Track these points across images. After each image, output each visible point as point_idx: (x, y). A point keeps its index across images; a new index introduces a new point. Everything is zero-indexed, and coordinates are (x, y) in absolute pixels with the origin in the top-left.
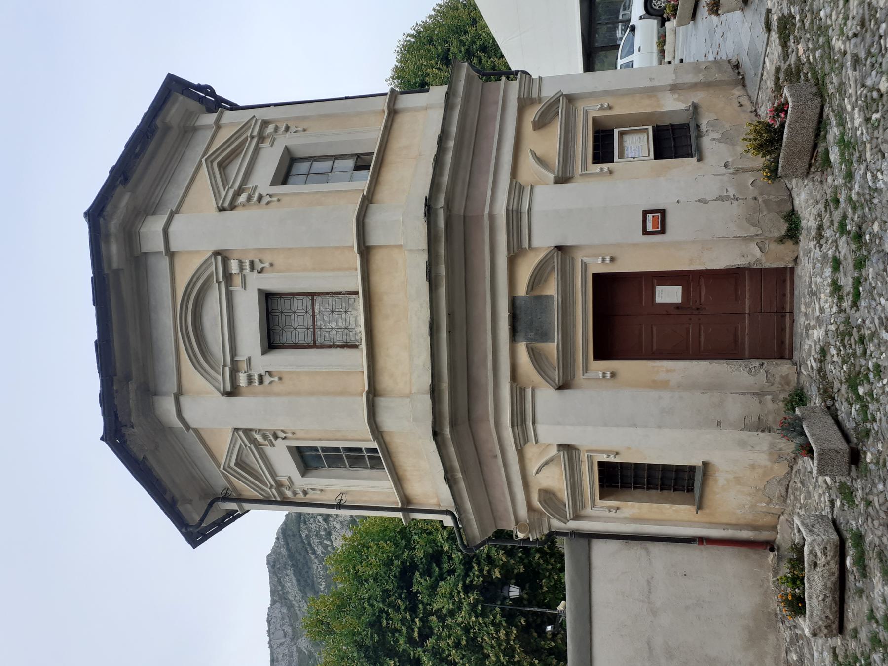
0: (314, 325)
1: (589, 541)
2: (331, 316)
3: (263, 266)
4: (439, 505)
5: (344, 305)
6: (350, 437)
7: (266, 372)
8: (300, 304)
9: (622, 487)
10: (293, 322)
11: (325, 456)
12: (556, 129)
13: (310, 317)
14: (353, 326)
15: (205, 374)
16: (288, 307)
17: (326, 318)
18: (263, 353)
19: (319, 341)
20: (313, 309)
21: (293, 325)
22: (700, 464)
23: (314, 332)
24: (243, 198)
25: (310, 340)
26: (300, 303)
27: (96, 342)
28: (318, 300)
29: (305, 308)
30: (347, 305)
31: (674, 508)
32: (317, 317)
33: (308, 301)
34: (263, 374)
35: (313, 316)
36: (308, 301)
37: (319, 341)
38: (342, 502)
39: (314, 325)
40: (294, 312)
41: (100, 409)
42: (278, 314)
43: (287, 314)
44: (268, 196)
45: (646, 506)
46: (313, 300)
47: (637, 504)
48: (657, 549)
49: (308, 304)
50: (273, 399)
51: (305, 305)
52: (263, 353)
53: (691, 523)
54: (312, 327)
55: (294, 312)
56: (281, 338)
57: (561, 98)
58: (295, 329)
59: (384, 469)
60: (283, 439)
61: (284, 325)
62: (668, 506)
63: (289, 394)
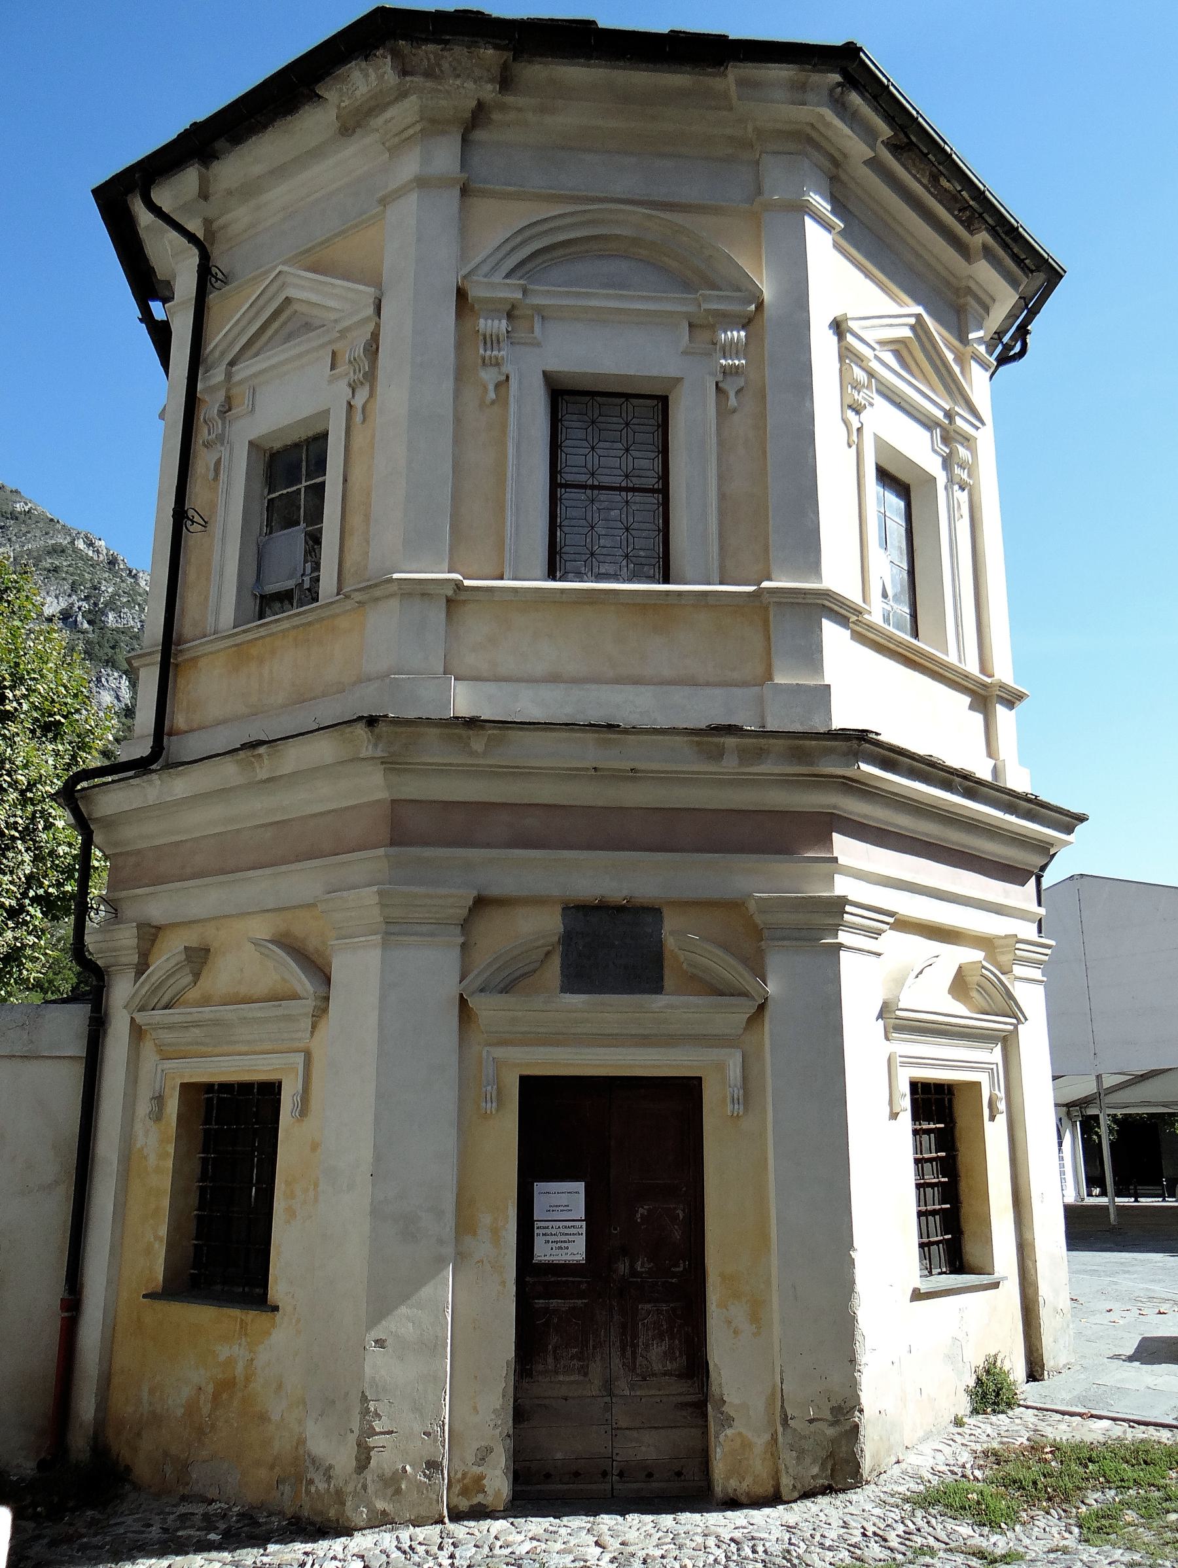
0: (600, 488)
1: (80, 1058)
2: (620, 525)
3: (732, 395)
4: (170, 734)
5: (642, 553)
6: (347, 544)
7: (508, 377)
8: (645, 464)
9: (207, 1132)
10: (607, 445)
11: (299, 489)
12: (957, 1010)
13: (618, 481)
14: (595, 570)
15: (508, 247)
16: (640, 437)
17: (614, 513)
18: (546, 375)
19: (566, 496)
20: (634, 490)
21: (601, 445)
22: (826, 683)
23: (584, 487)
24: (859, 374)
25: (569, 478)
26: (646, 464)
27: (594, 22)
28: (654, 499)
29: (636, 472)
30: (643, 561)
31: (157, 1246)
32: (618, 497)
33: (652, 481)
34: (504, 369)
35: (620, 489)
36: (652, 481)
37: (566, 496)
38: (189, 523)
39: (600, 488)
40: (627, 450)
41: (450, 8)
42: (590, 438)
43: (624, 435)
44: (860, 426)
45: (165, 1183)
46: (652, 491)
47: (169, 1164)
48: (58, 1206)
49: (643, 480)
50: (448, 384)
51: (642, 473)
52: (546, 375)
53: (113, 1282)
54: (596, 483)
55: (627, 450)
56: (575, 417)
57: (1014, 1021)
58: (593, 448)
59: (260, 619)
60: (349, 403)
61: (602, 426)
62: (163, 1231)
63: (458, 420)
